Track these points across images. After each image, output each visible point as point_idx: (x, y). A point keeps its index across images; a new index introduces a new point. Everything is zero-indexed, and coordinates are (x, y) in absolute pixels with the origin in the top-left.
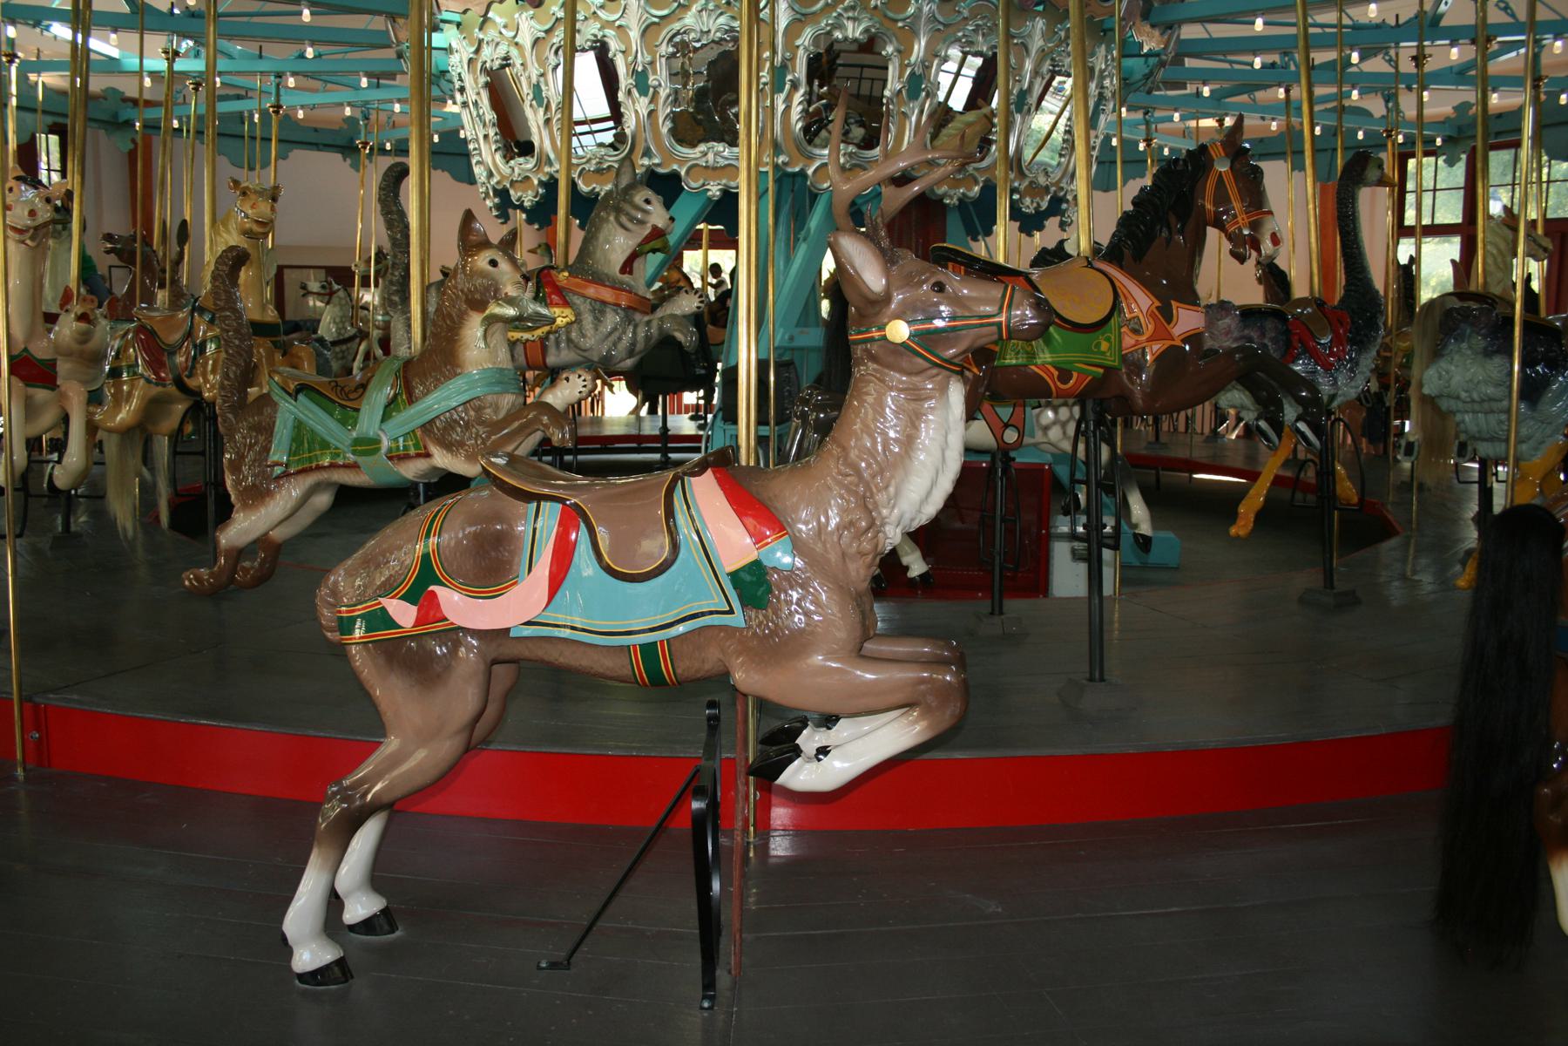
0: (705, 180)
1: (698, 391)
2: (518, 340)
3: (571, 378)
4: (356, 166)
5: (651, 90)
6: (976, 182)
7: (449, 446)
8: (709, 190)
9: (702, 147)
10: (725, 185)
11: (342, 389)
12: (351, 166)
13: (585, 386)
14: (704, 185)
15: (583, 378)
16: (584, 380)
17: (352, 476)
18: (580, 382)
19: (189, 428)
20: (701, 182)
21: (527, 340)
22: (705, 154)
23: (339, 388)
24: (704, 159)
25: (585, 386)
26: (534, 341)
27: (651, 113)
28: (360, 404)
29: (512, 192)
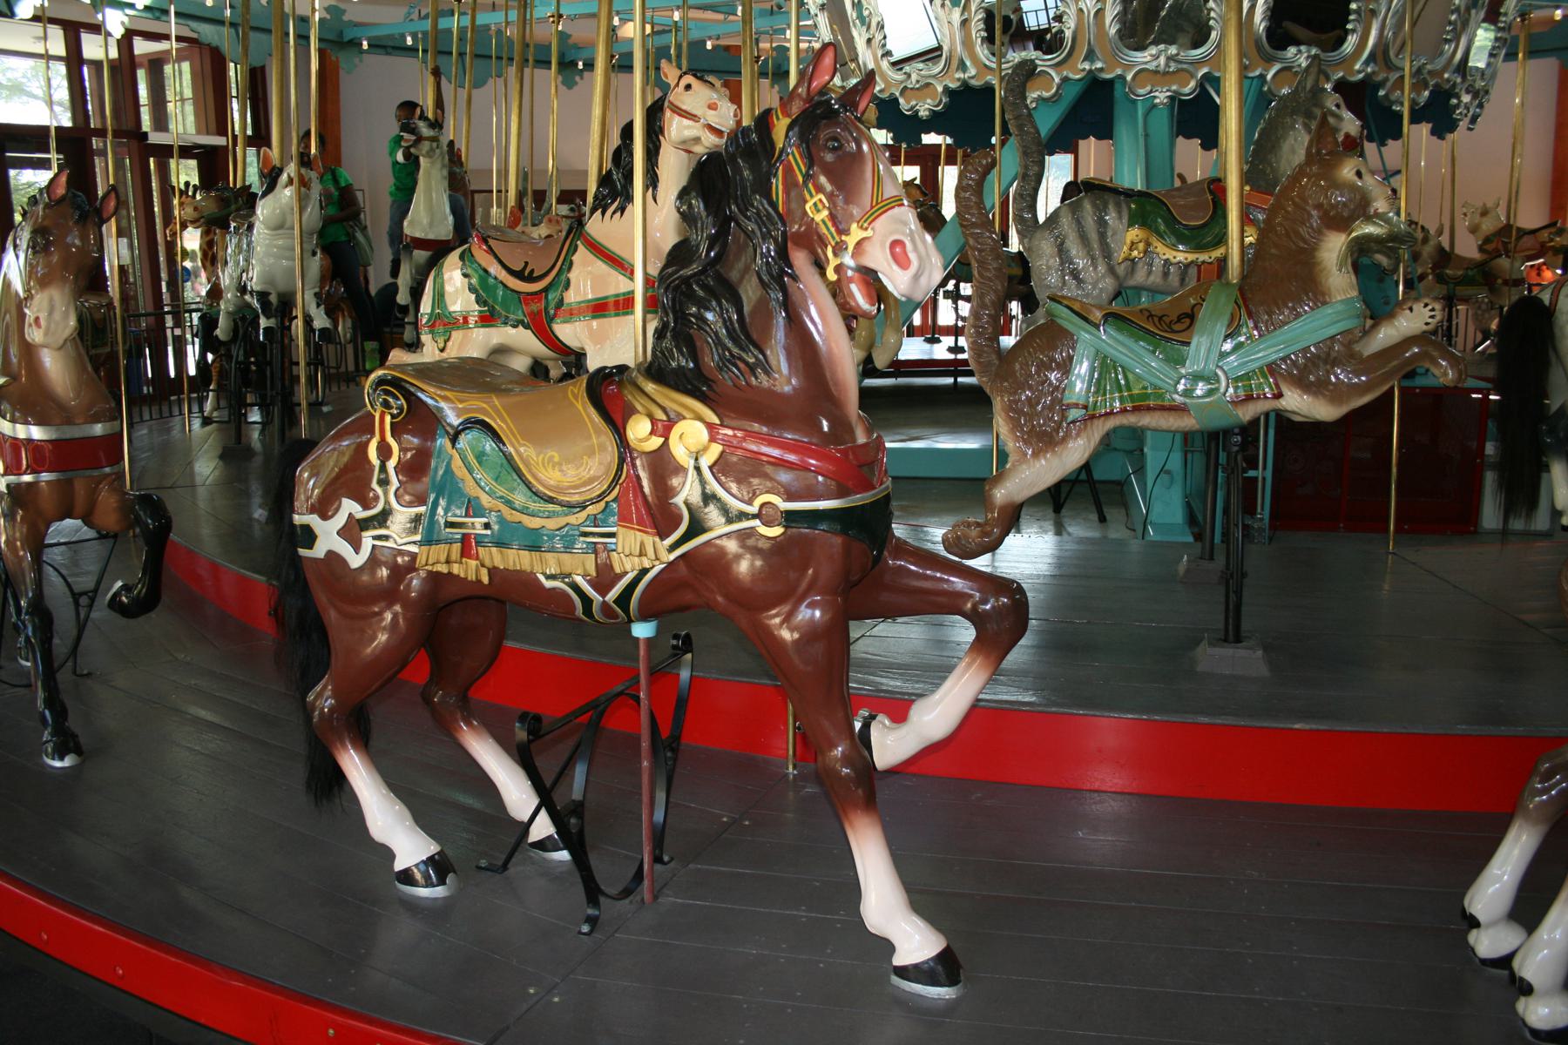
0: (1153, 86)
2: (1192, 262)
3: (1415, 307)
6: (1426, 87)
7: (1302, 383)
8: (1155, 97)
9: (1153, 50)
10: (1174, 92)
11: (1160, 318)
13: (1432, 317)
14: (1151, 92)
15: (1430, 307)
16: (1433, 310)
17: (1171, 420)
18: (1426, 312)
19: (210, 357)
20: (1149, 88)
21: (1203, 262)
22: (1157, 57)
23: (1156, 319)
24: (1155, 63)
25: (1432, 317)
26: (1210, 263)
28: (1191, 338)
29: (901, 101)
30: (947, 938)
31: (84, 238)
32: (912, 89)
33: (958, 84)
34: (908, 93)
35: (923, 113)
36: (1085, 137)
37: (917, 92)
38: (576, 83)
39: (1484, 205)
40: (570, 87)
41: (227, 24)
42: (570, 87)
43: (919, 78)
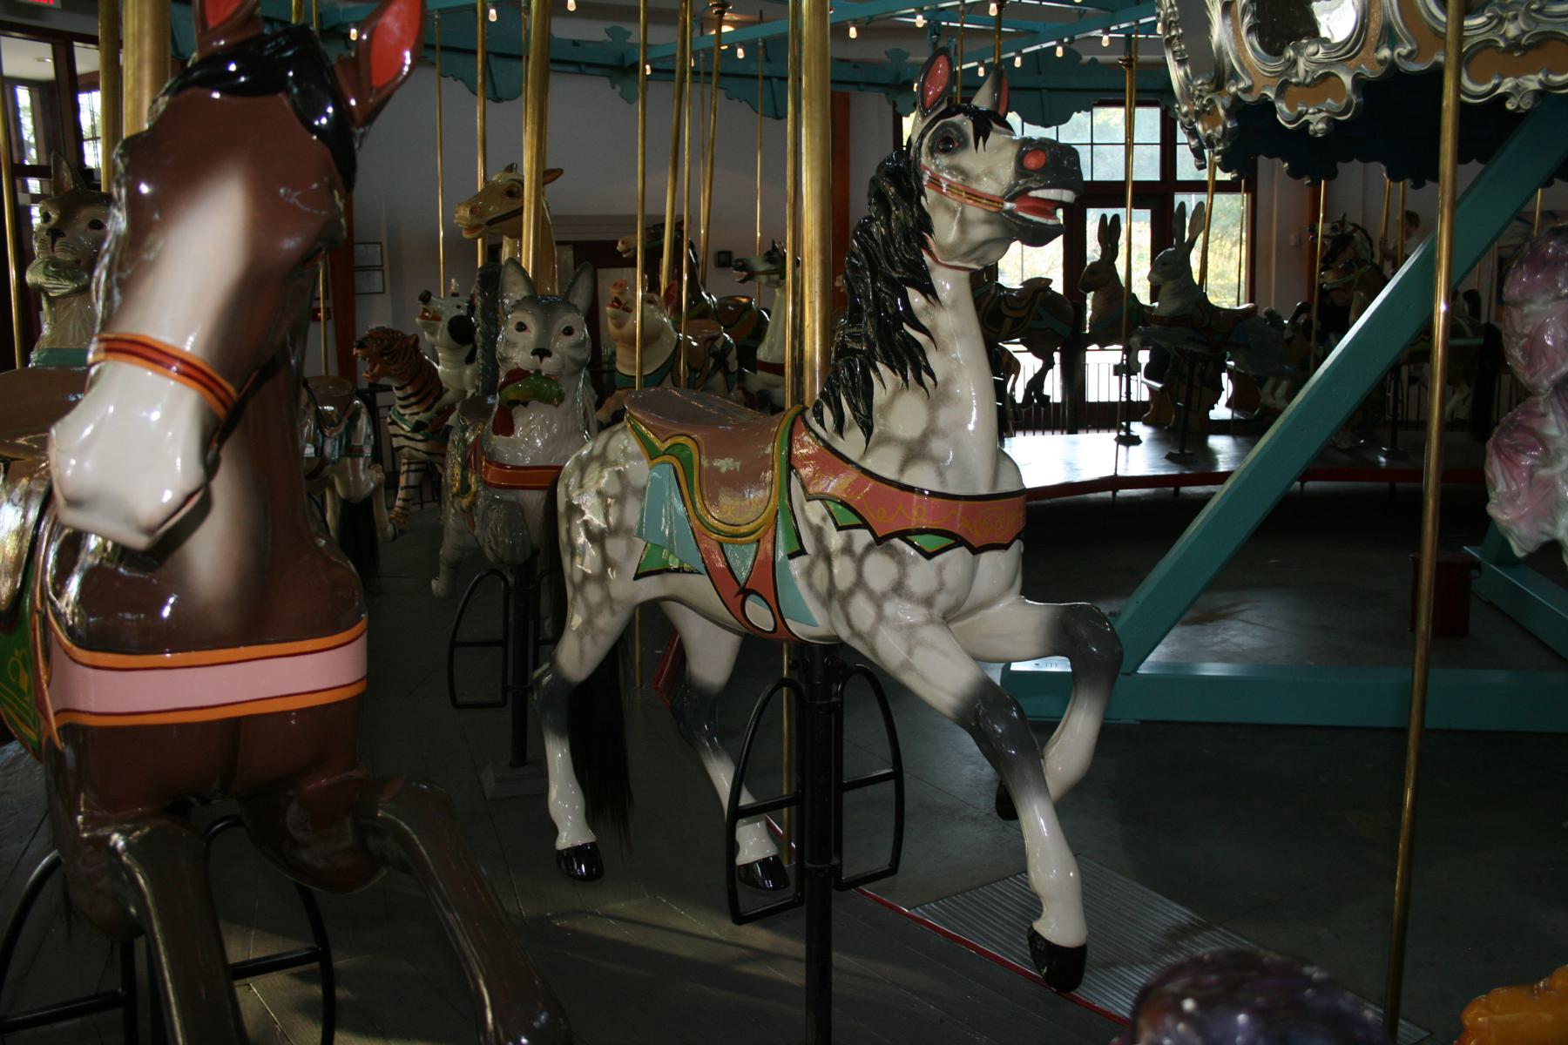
12: (622, 95)
30: (1091, 934)
32: (1297, 84)
33: (1381, 70)
34: (1292, 89)
35: (1318, 126)
36: (1348, 160)
37: (1305, 89)
39: (1025, 435)
41: (438, 48)
43: (1313, 66)
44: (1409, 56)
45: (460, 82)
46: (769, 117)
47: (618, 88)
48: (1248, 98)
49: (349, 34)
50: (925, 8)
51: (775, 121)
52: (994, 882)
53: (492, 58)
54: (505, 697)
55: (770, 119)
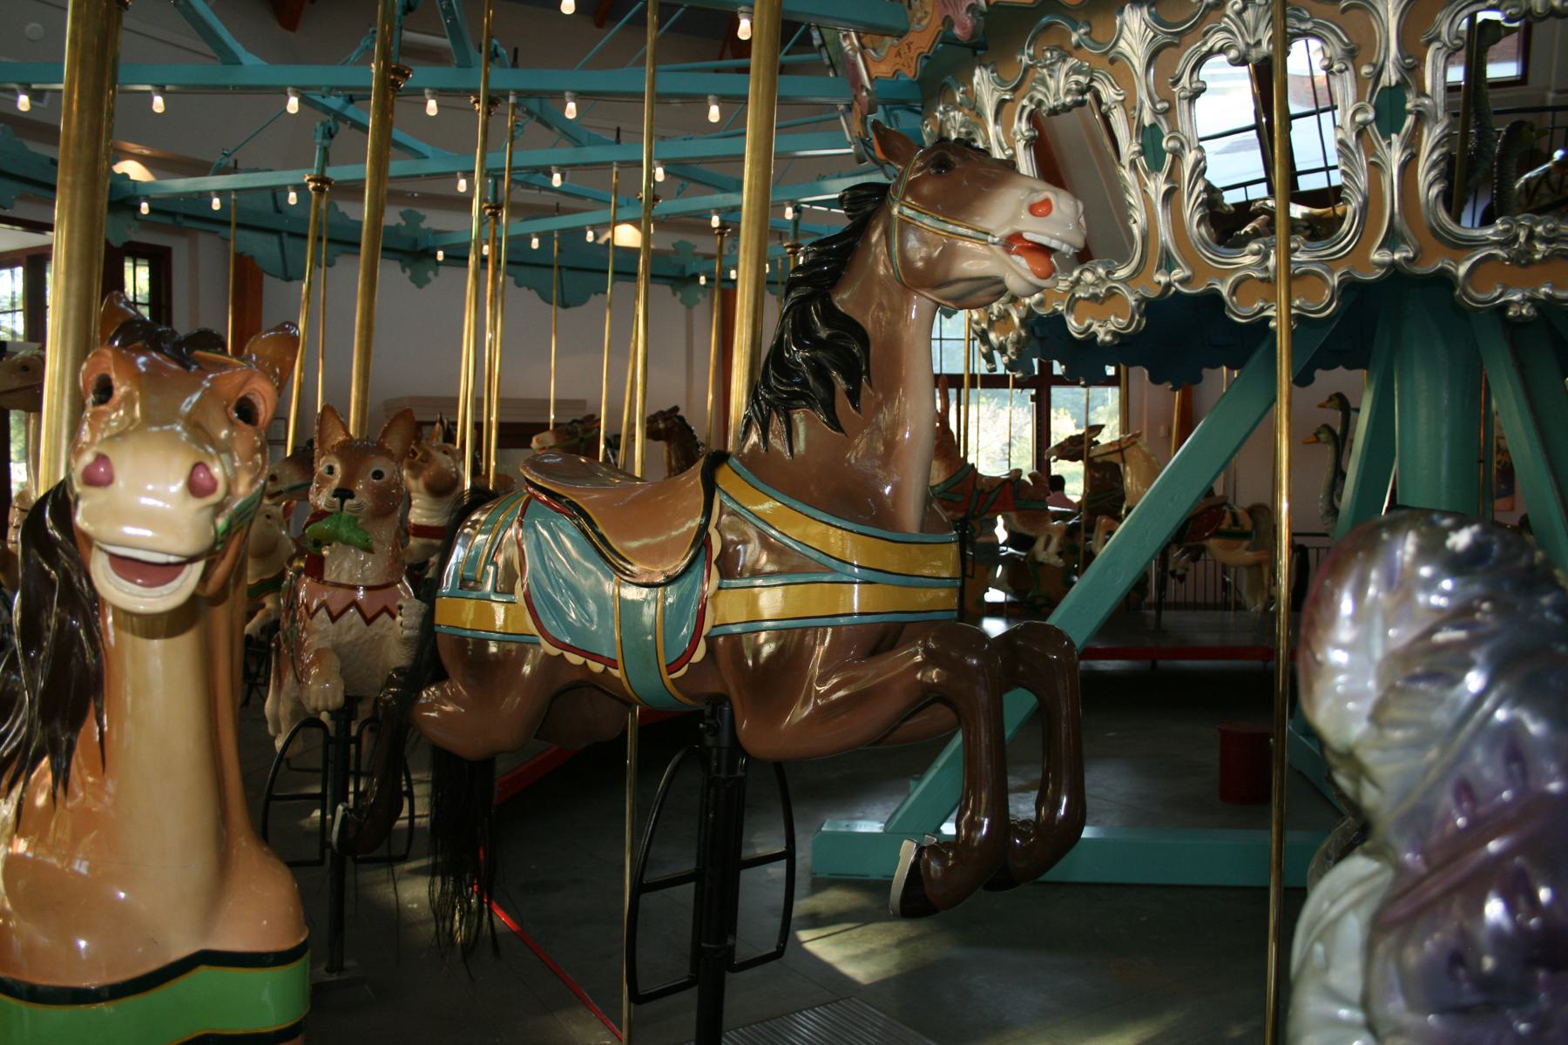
1: (1416, 855)
4: (419, 281)
5: (1169, 157)
12: (413, 279)
27: (1168, 195)
31: (259, 666)
35: (1103, 336)
38: (428, 281)
40: (420, 286)
42: (420, 286)
44: (1183, 282)
45: (533, 291)
46: (275, 276)
47: (408, 272)
48: (1042, 312)
49: (139, 208)
50: (168, 88)
51: (283, 282)
52: (768, 1020)
53: (564, 270)
54: (322, 853)
55: (279, 280)
